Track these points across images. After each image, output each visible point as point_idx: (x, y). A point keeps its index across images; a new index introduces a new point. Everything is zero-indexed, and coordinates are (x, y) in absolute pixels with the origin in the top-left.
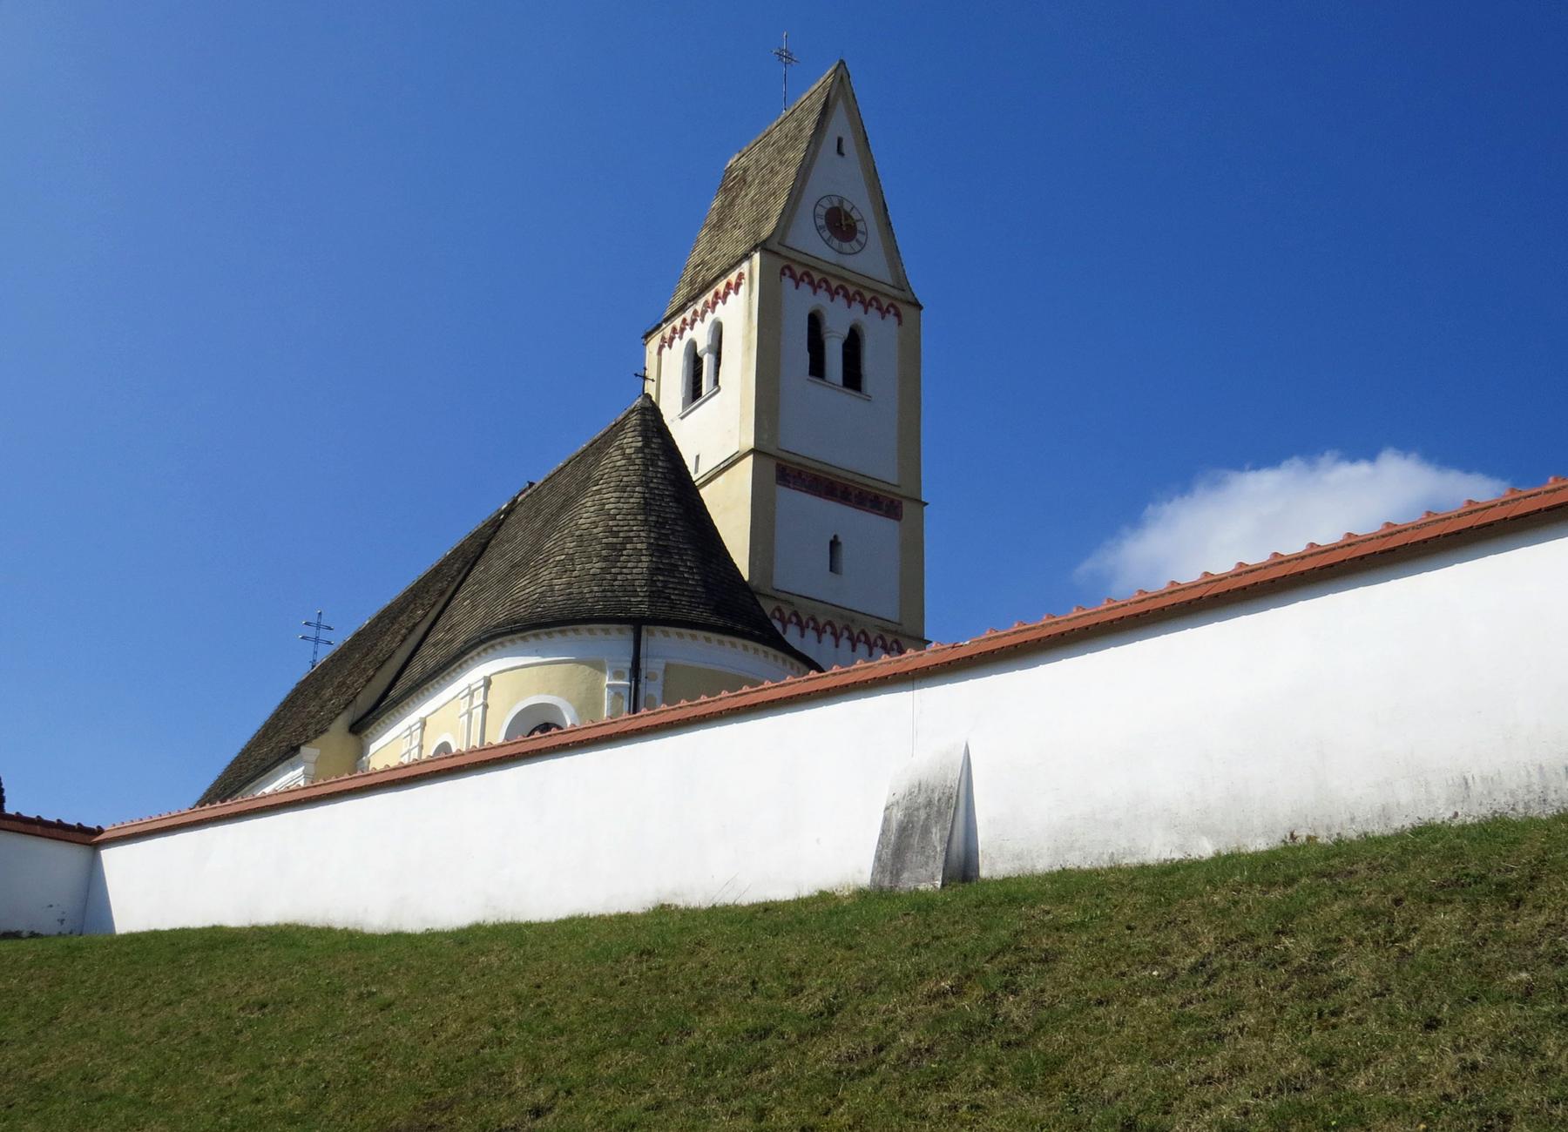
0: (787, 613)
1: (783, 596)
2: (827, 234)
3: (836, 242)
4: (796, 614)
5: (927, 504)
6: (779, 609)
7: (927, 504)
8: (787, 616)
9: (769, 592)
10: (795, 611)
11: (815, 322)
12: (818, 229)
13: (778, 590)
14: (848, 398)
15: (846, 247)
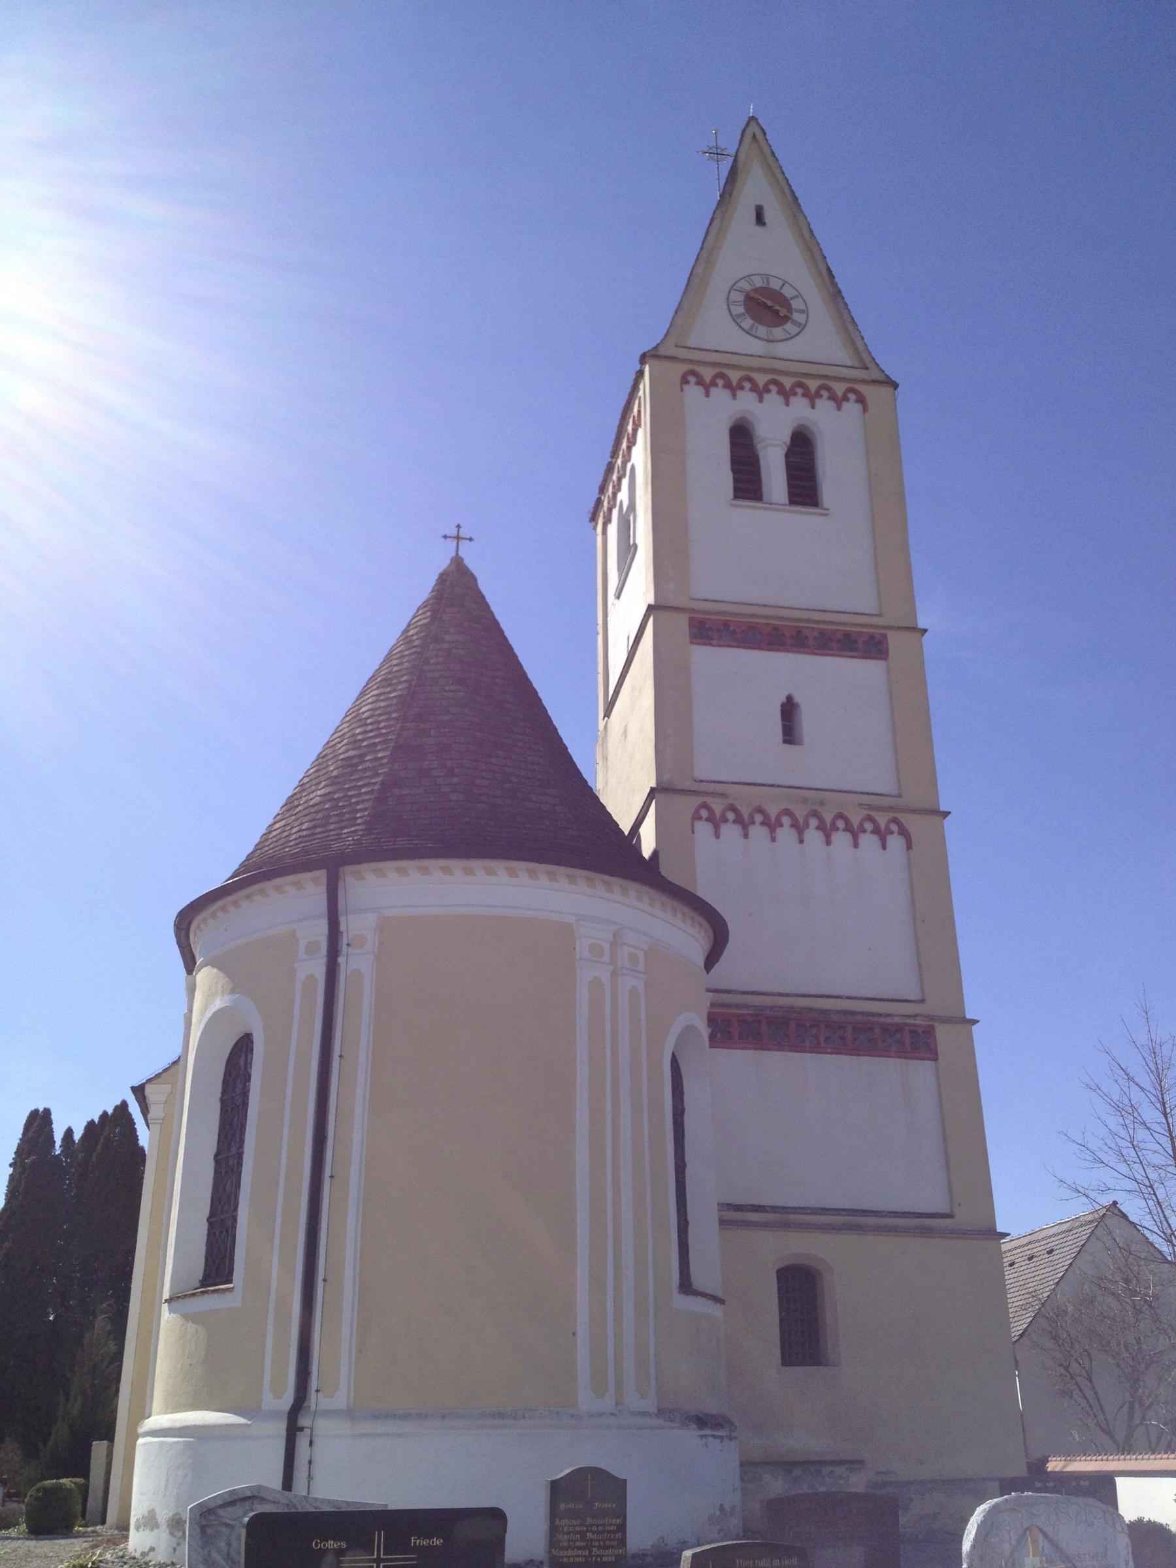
0: (718, 808)
1: (712, 787)
2: (748, 322)
3: (762, 330)
4: (732, 808)
5: (975, 1022)
6: (705, 806)
7: (975, 1022)
9: (688, 785)
10: (816, 811)
12: (735, 318)
13: (701, 781)
14: (803, 518)
15: (778, 332)
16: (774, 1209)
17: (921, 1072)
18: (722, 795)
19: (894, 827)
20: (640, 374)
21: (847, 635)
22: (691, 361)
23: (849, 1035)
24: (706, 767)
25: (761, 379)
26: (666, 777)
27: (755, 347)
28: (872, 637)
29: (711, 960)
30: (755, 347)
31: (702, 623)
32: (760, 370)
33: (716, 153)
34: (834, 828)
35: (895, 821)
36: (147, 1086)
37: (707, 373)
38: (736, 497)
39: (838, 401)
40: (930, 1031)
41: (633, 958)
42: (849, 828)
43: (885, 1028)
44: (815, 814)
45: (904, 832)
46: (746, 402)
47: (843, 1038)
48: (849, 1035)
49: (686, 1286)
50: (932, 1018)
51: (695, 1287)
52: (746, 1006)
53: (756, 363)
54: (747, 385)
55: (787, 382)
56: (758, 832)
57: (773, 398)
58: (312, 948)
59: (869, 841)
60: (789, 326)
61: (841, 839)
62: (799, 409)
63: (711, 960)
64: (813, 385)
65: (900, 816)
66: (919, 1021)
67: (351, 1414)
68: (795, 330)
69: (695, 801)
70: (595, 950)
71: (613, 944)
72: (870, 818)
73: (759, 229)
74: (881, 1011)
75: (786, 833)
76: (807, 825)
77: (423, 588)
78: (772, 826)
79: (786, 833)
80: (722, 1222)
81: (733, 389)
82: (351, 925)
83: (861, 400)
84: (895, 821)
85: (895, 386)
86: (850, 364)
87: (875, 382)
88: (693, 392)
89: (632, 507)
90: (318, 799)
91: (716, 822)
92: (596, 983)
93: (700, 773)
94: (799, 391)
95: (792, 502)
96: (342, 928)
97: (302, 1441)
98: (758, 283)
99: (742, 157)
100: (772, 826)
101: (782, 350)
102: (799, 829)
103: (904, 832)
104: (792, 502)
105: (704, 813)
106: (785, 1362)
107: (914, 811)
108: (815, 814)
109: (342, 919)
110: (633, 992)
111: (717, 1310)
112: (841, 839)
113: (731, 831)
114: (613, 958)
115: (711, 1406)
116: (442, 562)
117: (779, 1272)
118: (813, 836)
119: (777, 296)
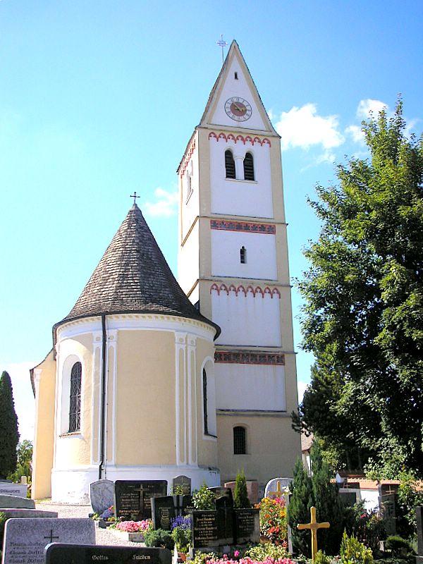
2: (231, 115)
3: (236, 118)
8: (218, 136)
9: (210, 278)
11: (229, 155)
14: (249, 183)
15: (242, 118)
16: (233, 410)
17: (279, 368)
18: (221, 281)
19: (275, 291)
20: (195, 132)
21: (262, 226)
22: (212, 129)
23: (258, 358)
24: (216, 271)
25: (236, 135)
26: (202, 275)
27: (234, 123)
28: (270, 226)
29: (216, 337)
30: (234, 123)
31: (215, 222)
32: (235, 132)
33: (222, 43)
34: (256, 291)
35: (276, 289)
36: (35, 370)
37: (218, 133)
38: (227, 177)
39: (262, 143)
40: (283, 356)
41: (192, 341)
42: (261, 292)
43: (269, 356)
44: (250, 287)
45: (278, 293)
46: (230, 144)
47: (256, 360)
48: (258, 358)
49: (206, 433)
50: (284, 352)
51: (202, 312)
52: (227, 350)
53: (235, 129)
54: (231, 137)
55: (245, 137)
56: (232, 293)
57: (240, 142)
58: (98, 339)
59: (267, 295)
60: (245, 116)
61: (259, 295)
62: (248, 147)
63: (216, 337)
64: (253, 137)
65: (277, 287)
66: (280, 353)
67: (116, 466)
68: (247, 117)
69: (212, 283)
70: (181, 340)
71: (186, 338)
72: (268, 288)
73: (236, 80)
74: (193, 455)
75: (241, 293)
76: (248, 291)
77: (124, 216)
78: (236, 291)
79: (241, 293)
80: (217, 414)
81: (226, 139)
82: (109, 333)
83: (269, 143)
84: (276, 289)
85: (281, 137)
86: (265, 129)
87: (274, 136)
88: (213, 139)
89: (192, 173)
90: (96, 291)
91: (218, 290)
92: (181, 350)
93: (213, 274)
94: (248, 139)
95: (246, 179)
96: (107, 334)
97: (103, 473)
98: (235, 100)
99: (230, 55)
100: (236, 291)
101: (244, 125)
102: (245, 292)
103: (278, 293)
104: (246, 179)
105: (215, 287)
106: (235, 453)
107: (282, 286)
108: (250, 287)
109: (107, 331)
110: (192, 352)
111: (215, 440)
112: (259, 295)
113: (223, 292)
114: (186, 343)
115: (212, 465)
116: (131, 208)
117: (234, 429)
118: (250, 294)
119: (241, 105)
